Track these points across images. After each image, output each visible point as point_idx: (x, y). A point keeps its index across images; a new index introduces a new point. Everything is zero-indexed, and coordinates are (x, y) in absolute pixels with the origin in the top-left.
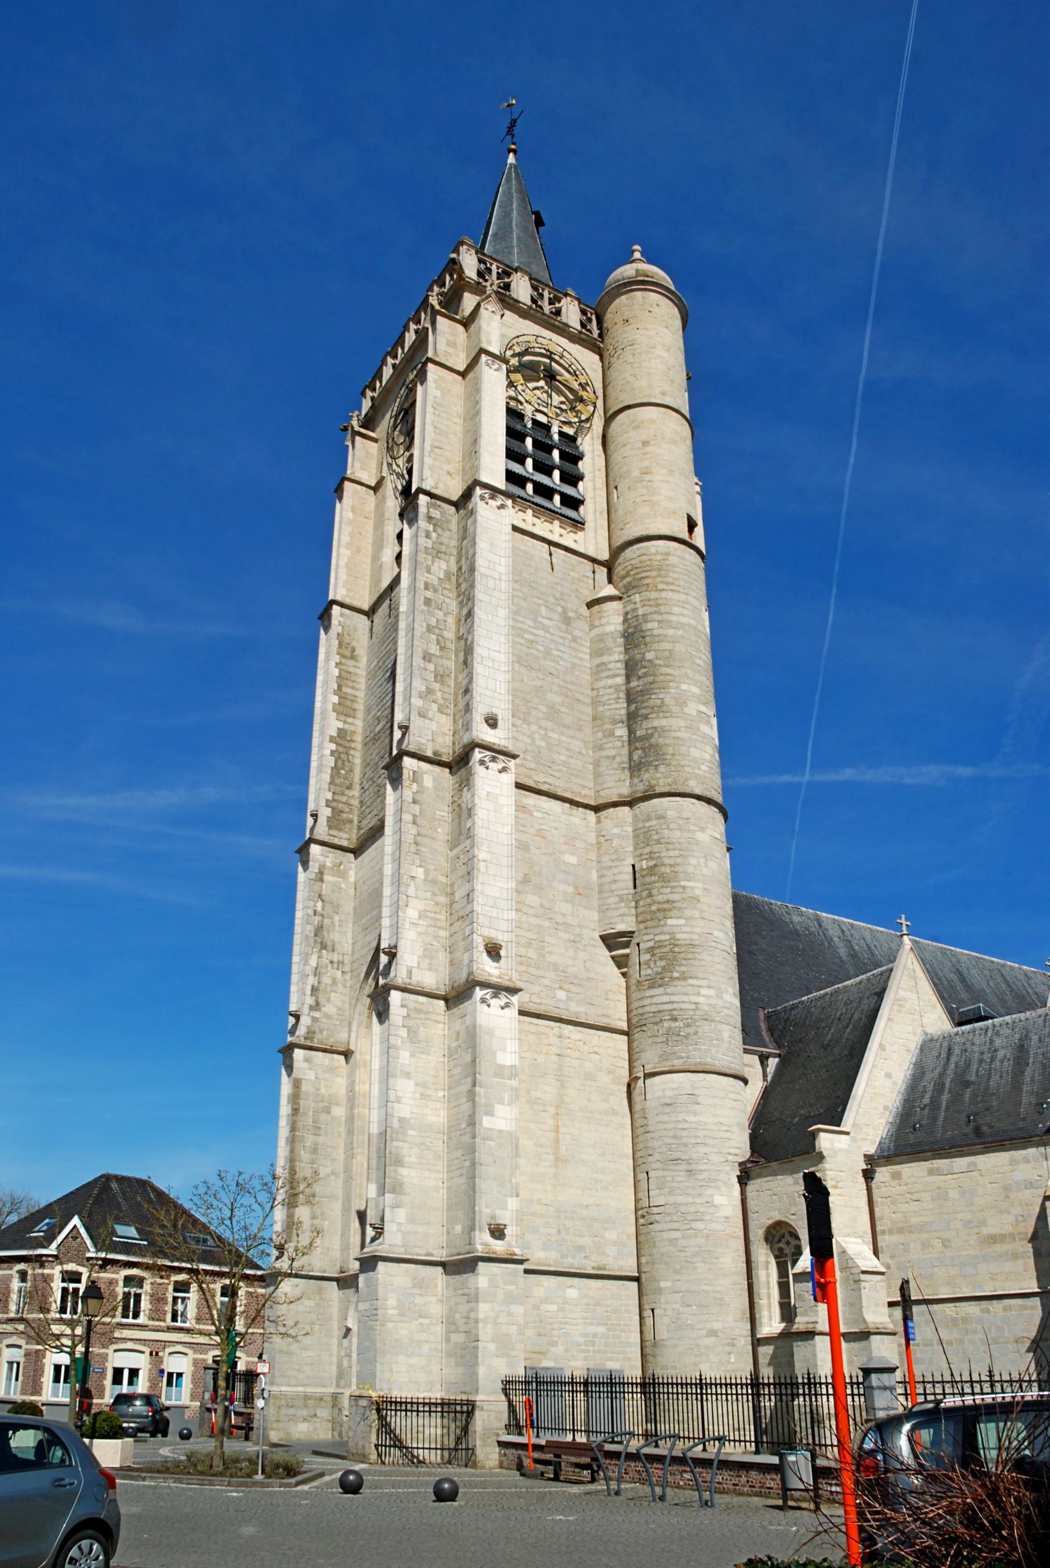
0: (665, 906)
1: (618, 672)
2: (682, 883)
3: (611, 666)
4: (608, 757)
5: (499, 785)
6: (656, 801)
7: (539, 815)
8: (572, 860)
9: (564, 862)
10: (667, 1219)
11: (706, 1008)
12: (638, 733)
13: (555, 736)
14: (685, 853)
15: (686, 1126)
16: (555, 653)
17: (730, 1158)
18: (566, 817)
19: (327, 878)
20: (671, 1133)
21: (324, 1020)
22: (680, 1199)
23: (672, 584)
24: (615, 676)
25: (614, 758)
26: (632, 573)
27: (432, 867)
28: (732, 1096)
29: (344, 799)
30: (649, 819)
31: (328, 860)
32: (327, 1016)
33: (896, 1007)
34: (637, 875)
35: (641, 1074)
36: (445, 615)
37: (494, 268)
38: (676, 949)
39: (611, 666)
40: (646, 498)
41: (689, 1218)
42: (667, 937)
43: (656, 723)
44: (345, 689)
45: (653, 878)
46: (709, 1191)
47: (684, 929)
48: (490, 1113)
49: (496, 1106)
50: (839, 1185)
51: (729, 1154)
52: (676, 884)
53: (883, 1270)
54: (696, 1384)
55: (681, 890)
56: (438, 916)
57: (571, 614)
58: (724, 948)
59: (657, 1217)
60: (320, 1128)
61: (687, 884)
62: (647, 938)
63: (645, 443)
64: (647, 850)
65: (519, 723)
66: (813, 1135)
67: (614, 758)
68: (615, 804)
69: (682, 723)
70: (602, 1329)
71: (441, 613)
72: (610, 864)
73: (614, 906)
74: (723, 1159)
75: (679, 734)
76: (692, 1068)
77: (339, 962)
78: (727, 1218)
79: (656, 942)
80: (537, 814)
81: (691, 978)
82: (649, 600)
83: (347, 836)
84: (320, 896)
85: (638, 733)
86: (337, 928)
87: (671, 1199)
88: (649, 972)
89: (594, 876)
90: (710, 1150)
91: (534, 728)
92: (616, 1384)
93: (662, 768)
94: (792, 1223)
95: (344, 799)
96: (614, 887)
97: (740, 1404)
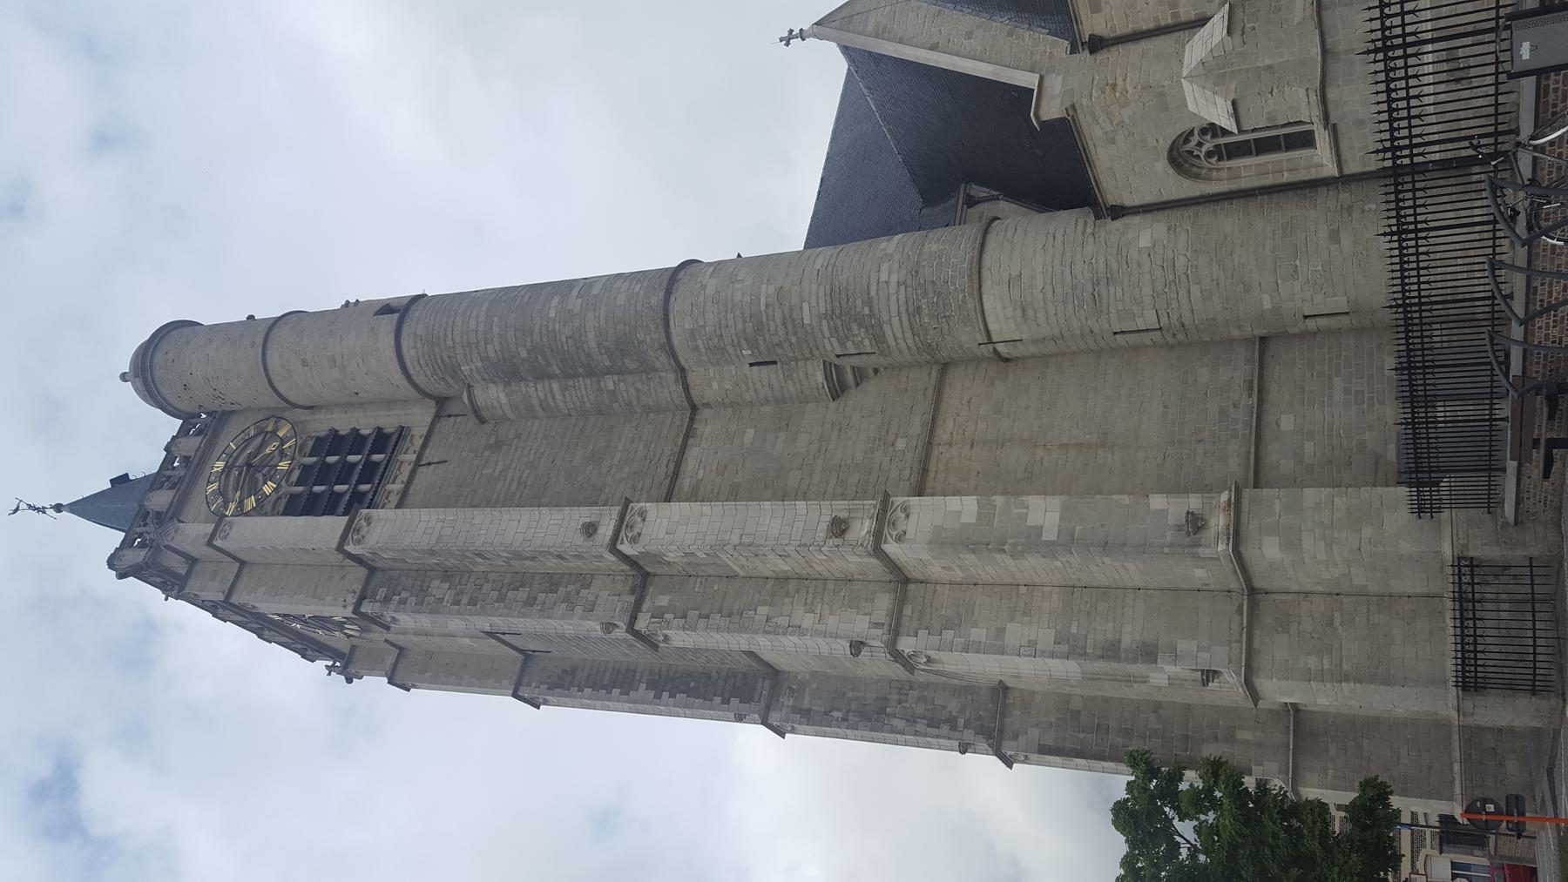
0: (790, 327)
1: (547, 388)
2: (763, 308)
3: (542, 395)
4: (638, 398)
5: (659, 520)
6: (676, 342)
7: (701, 472)
8: (750, 433)
9: (752, 444)
10: (1174, 305)
11: (903, 273)
12: (607, 363)
13: (618, 455)
14: (730, 306)
15: (1049, 289)
16: (532, 456)
17: (1089, 230)
18: (704, 442)
19: (806, 703)
20: (1061, 307)
21: (967, 714)
22: (1147, 290)
23: (445, 330)
24: (551, 390)
25: (637, 390)
26: (440, 374)
27: (757, 596)
28: (1010, 234)
29: (721, 683)
30: (696, 349)
31: (786, 703)
32: (962, 709)
33: (886, 35)
34: (761, 360)
35: (990, 347)
36: (488, 581)
37: (138, 530)
38: (838, 311)
39: (542, 395)
40: (360, 361)
41: (1171, 278)
42: (824, 322)
43: (593, 345)
44: (606, 682)
45: (761, 342)
46: (1134, 254)
47: (814, 304)
48: (1038, 530)
49: (1028, 524)
50: (1110, 82)
51: (1083, 233)
52: (764, 314)
53: (1227, 6)
54: (1400, 241)
55: (770, 309)
56: (811, 590)
57: (492, 441)
58: (835, 255)
59: (1174, 318)
60: (1099, 725)
61: (763, 303)
62: (828, 347)
63: (305, 364)
64: (731, 350)
65: (603, 497)
66: (1043, 124)
67: (637, 390)
68: (686, 387)
69: (591, 315)
70: (1337, 381)
71: (485, 585)
72: (752, 393)
73: (798, 385)
74: (1091, 239)
75: (602, 318)
76: (976, 286)
77: (899, 693)
78: (1169, 229)
79: (832, 336)
80: (700, 475)
81: (869, 294)
82: (465, 355)
83: (760, 680)
84: (826, 713)
85: (607, 363)
86: (860, 694)
87: (1147, 301)
88: (866, 342)
89: (767, 409)
90: (1079, 257)
91: (609, 479)
92: (1409, 362)
93: (641, 336)
94: (1170, 142)
95: (721, 683)
96: (776, 387)
97: (1433, 264)
